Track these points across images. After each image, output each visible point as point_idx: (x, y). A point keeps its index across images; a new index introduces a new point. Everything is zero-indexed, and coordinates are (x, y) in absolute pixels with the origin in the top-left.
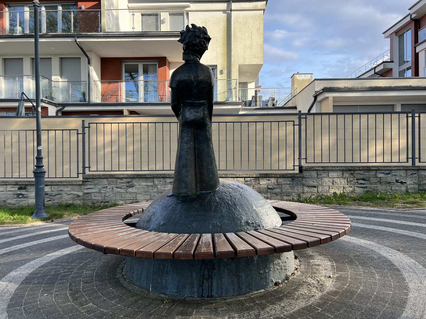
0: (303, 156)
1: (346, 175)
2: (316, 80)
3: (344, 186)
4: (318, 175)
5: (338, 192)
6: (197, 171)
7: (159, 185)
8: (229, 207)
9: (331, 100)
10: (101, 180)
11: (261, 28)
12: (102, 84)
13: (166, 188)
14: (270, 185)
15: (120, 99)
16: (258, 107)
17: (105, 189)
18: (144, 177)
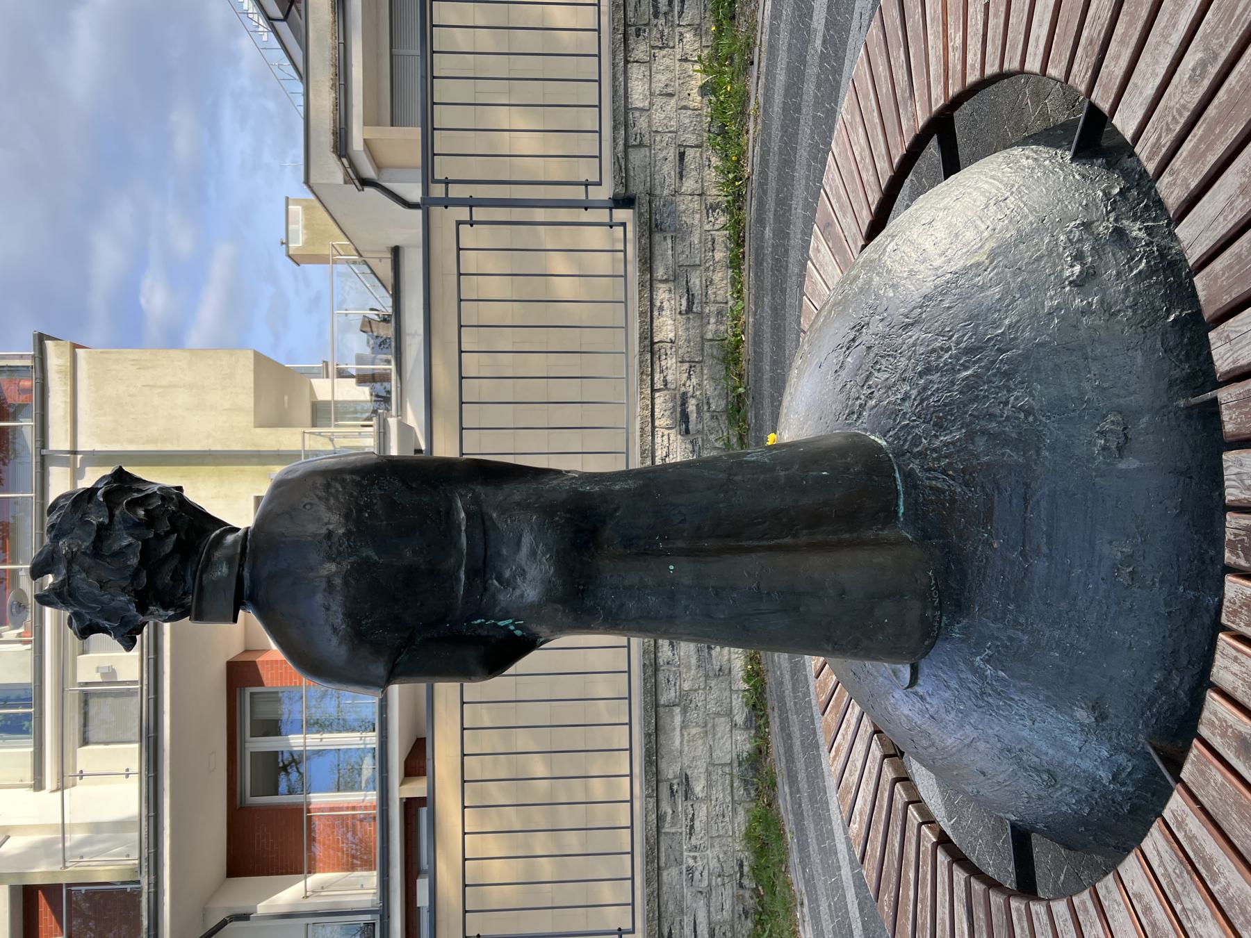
0: (578, 193)
1: (640, 50)
2: (307, 182)
3: (680, 60)
4: (641, 145)
5: (699, 79)
6: (803, 539)
7: (680, 685)
8: (995, 375)
9: (375, 133)
10: (664, 889)
11: (136, 357)
12: (315, 869)
13: (690, 662)
14: (678, 304)
15: (366, 808)
16: (393, 367)
17: (697, 874)
18: (653, 738)
